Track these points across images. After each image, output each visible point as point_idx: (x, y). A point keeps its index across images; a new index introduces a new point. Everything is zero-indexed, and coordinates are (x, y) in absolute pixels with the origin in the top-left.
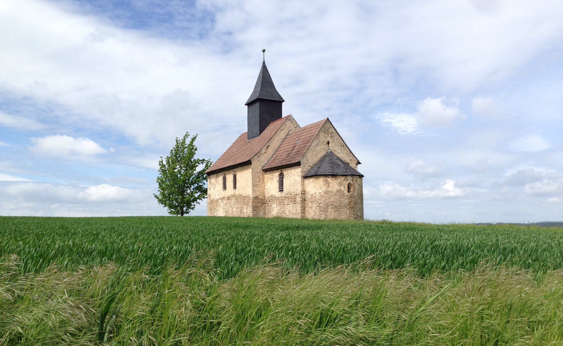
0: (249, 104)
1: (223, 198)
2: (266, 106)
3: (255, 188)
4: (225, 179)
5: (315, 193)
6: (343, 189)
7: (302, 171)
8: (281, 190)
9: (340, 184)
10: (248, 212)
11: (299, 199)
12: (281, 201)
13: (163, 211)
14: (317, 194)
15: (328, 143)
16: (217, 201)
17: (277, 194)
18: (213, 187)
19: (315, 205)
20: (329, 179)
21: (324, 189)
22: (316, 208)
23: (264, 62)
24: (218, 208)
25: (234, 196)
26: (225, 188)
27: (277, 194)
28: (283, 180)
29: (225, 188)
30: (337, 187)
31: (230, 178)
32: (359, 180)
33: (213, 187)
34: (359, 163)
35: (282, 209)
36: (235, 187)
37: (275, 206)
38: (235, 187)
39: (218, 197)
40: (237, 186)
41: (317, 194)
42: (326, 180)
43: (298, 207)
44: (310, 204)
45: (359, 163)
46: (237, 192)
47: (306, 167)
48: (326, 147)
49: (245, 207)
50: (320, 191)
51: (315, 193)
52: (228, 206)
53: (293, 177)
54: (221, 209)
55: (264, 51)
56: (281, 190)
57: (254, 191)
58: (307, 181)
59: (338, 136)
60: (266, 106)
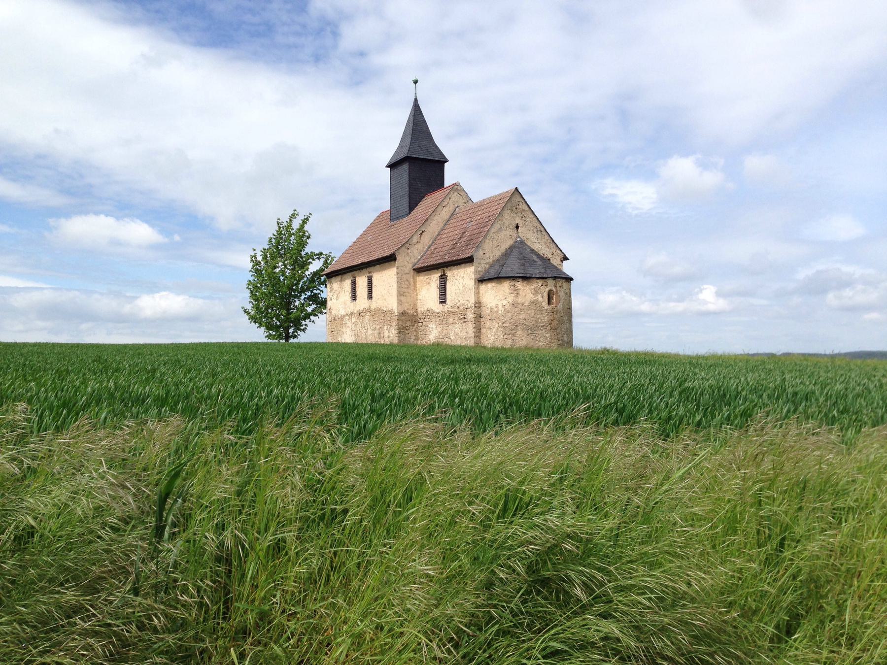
0: (392, 166)
1: (352, 314)
2: (419, 168)
3: (402, 298)
4: (354, 283)
5: (497, 306)
6: (540, 299)
7: (476, 272)
8: (443, 300)
9: (536, 292)
10: (390, 335)
11: (470, 316)
12: (443, 319)
13: (257, 334)
14: (500, 307)
15: (517, 227)
16: (342, 318)
17: (437, 307)
18: (335, 296)
19: (497, 325)
20: (519, 284)
21: (511, 299)
22: (498, 330)
23: (416, 100)
24: (344, 330)
25: (369, 310)
26: (354, 297)
27: (437, 307)
28: (445, 286)
29: (354, 297)
30: (531, 296)
31: (362, 281)
32: (565, 285)
33: (335, 296)
34: (565, 258)
35: (445, 331)
36: (370, 297)
37: (434, 327)
38: (370, 297)
39: (343, 312)
40: (374, 295)
41: (500, 307)
42: (514, 286)
43: (470, 329)
44: (488, 324)
45: (565, 258)
46: (374, 304)
47: (483, 265)
48: (513, 233)
49: (385, 328)
50: (505, 302)
51: (497, 306)
52: (359, 326)
53: (461, 281)
54: (348, 331)
55: (416, 82)
56: (443, 300)
57: (400, 302)
58: (483, 287)
59: (532, 216)
60: (419, 168)
